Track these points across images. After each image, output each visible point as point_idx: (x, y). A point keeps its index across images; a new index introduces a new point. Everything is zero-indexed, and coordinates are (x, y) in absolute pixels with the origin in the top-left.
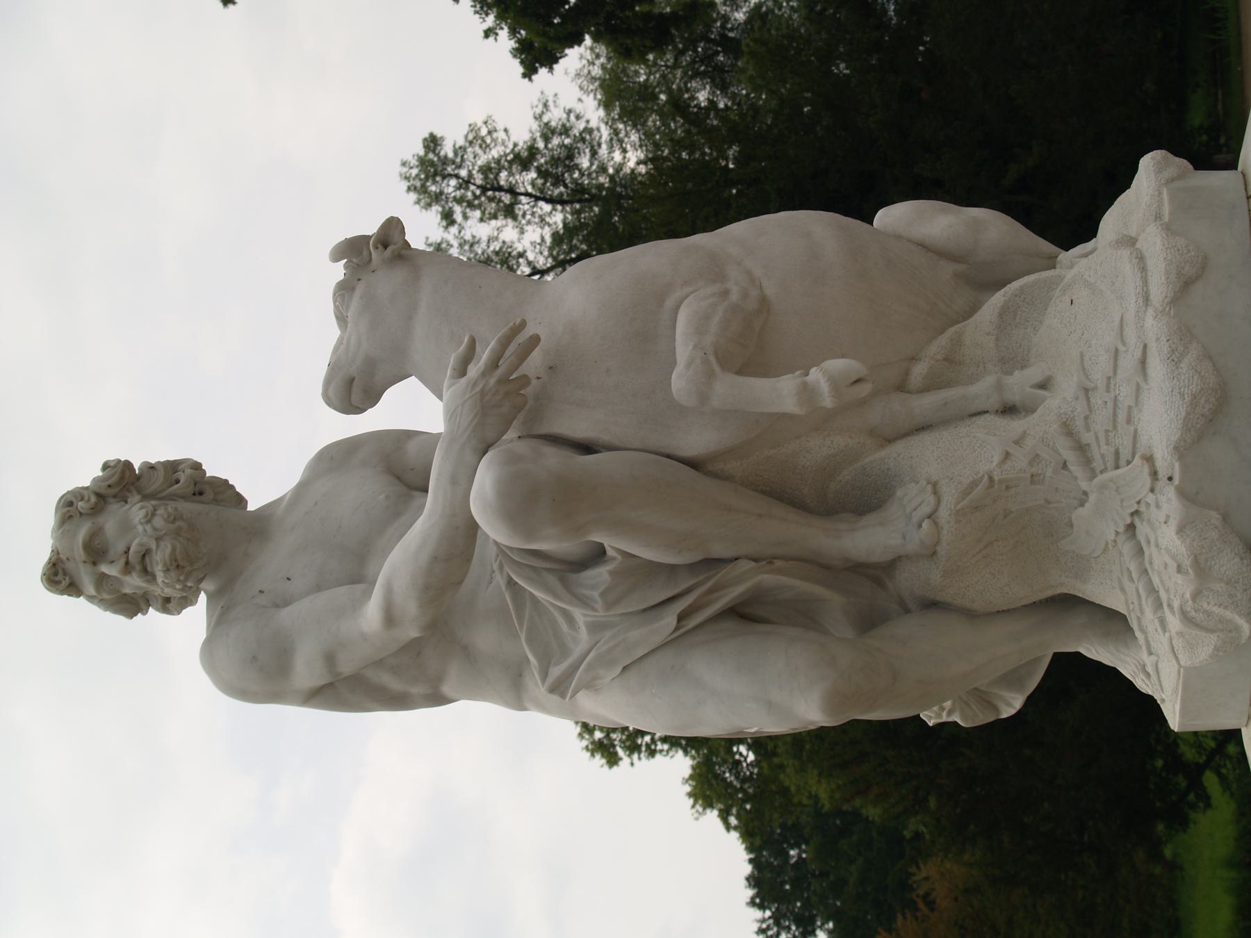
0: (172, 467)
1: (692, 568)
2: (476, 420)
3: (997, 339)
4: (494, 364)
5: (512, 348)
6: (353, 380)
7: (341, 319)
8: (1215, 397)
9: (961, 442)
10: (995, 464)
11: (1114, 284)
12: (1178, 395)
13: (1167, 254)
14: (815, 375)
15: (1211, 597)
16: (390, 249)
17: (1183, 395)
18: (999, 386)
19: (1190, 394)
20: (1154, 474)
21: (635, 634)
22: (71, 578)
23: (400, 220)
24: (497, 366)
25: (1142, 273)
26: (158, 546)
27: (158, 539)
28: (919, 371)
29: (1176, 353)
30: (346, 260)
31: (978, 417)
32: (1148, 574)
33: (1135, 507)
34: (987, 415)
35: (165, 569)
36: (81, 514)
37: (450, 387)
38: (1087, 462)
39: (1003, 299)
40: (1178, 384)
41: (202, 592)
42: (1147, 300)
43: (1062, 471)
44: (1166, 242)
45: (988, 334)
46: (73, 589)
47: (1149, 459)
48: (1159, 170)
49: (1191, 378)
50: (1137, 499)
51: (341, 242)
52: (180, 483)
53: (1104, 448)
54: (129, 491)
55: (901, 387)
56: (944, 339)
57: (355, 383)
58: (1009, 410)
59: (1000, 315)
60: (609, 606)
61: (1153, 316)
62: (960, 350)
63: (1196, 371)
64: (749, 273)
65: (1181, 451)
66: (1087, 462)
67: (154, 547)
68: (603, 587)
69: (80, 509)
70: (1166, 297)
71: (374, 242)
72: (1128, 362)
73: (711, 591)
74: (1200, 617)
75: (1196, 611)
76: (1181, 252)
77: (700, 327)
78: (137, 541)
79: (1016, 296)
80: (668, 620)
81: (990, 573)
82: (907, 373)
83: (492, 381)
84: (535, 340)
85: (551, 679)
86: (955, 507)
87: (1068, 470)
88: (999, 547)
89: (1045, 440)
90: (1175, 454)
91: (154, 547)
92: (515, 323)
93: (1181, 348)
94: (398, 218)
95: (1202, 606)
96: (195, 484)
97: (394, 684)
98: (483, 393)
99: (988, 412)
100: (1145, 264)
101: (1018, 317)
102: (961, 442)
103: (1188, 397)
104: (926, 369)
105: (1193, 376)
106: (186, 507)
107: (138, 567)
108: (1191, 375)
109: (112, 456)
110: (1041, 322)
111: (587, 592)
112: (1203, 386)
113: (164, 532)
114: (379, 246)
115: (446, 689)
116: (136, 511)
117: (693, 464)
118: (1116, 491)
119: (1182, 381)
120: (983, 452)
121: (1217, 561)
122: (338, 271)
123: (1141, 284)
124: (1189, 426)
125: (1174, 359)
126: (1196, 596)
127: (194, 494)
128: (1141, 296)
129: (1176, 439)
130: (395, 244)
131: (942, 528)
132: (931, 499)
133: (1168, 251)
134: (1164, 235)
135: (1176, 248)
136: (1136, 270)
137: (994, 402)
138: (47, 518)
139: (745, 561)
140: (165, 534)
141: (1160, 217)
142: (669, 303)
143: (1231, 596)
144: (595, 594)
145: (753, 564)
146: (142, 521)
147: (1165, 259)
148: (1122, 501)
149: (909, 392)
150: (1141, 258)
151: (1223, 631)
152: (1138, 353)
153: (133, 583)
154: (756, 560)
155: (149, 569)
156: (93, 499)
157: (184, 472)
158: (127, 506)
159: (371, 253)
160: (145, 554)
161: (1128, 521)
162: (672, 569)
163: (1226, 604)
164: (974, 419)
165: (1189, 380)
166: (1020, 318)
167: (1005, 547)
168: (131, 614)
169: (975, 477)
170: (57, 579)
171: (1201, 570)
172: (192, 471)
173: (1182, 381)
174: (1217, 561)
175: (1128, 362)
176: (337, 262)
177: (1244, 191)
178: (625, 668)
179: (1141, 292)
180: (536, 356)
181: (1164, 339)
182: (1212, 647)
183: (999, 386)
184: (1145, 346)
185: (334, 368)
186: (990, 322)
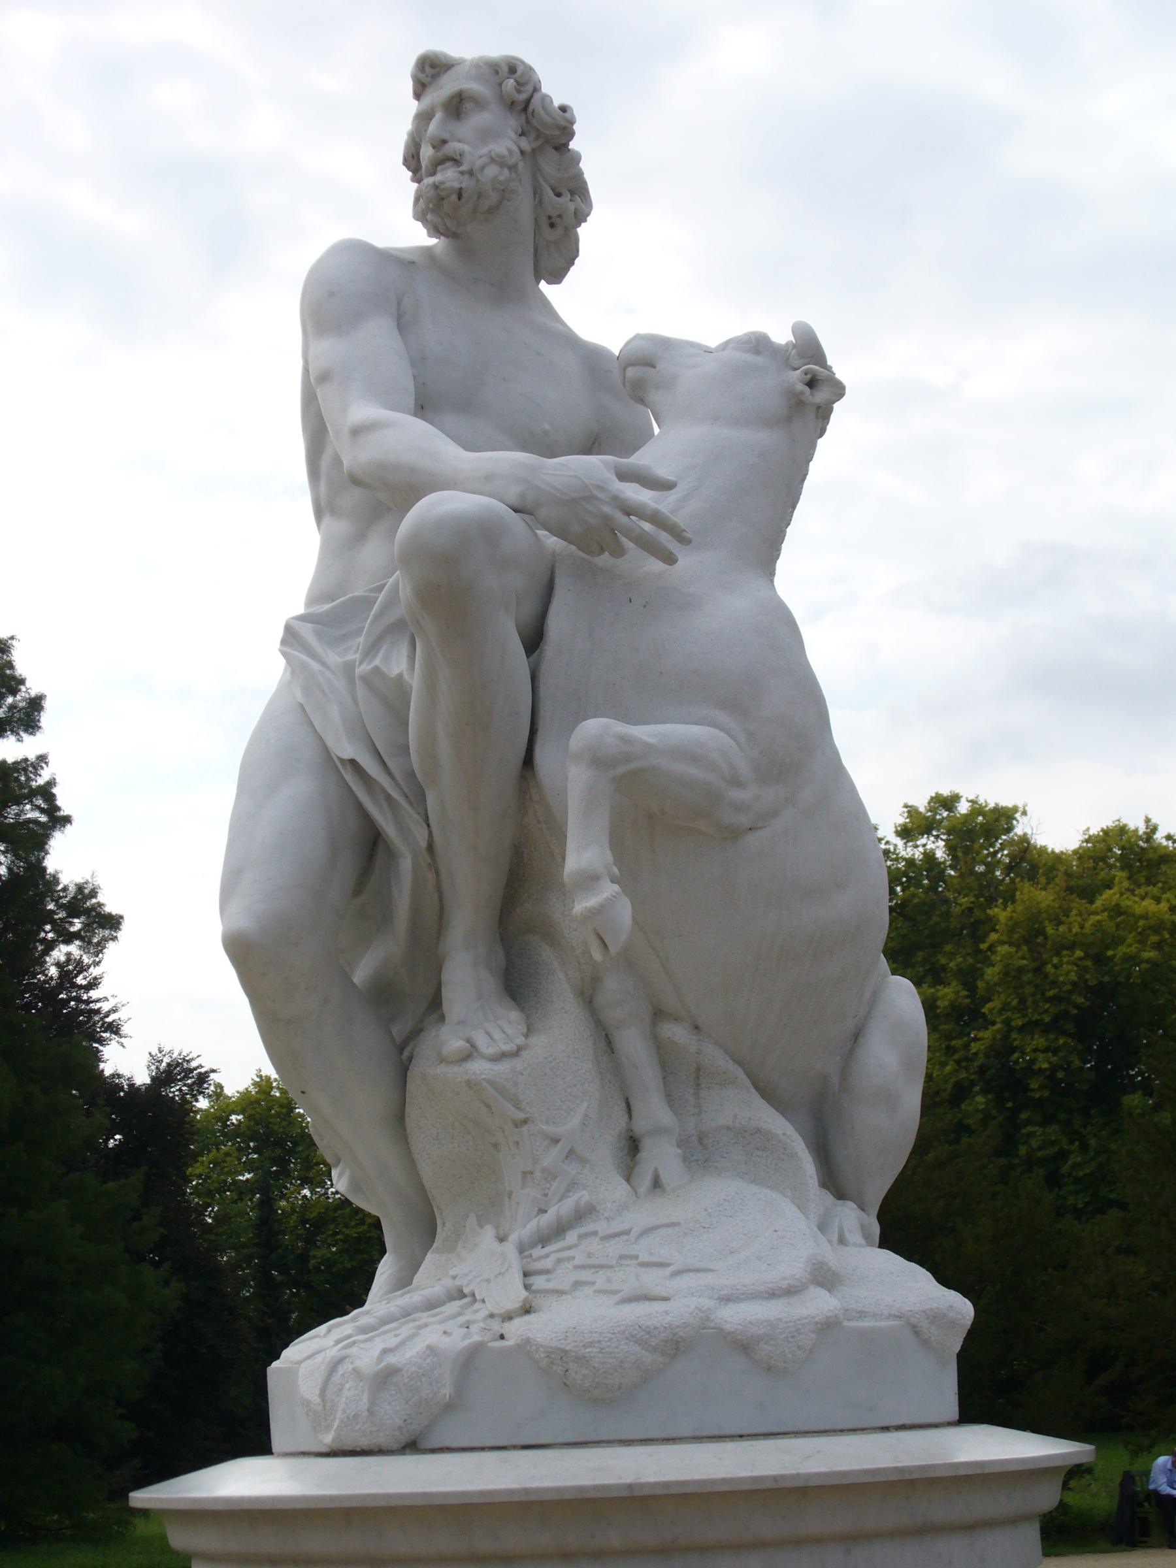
0: (577, 189)
1: (411, 774)
2: (558, 494)
3: (729, 1128)
4: (629, 510)
5: (647, 526)
6: (654, 367)
7: (725, 346)
8: (591, 1386)
9: (575, 1085)
10: (544, 1127)
11: (759, 1259)
12: (591, 1340)
13: (786, 1323)
14: (609, 889)
15: (356, 1392)
16: (807, 389)
17: (591, 1347)
18: (659, 1131)
19: (592, 1355)
20: (508, 1317)
21: (334, 712)
22: (431, 83)
23: (842, 397)
24: (629, 514)
25: (767, 1292)
26: (462, 173)
27: (471, 173)
28: (677, 1033)
29: (648, 1336)
30: (794, 342)
31: (625, 1108)
32: (404, 1317)
33: (478, 1297)
34: (626, 1117)
35: (437, 184)
36: (500, 84)
37: (603, 462)
38: (543, 1239)
39: (780, 1132)
40: (606, 1339)
41: (438, 240)
42: (727, 1299)
43: (537, 1209)
44: (806, 1321)
45: (735, 1116)
46: (420, 89)
47: (527, 1310)
48: (937, 1318)
49: (612, 1355)
50: (486, 1300)
51: (815, 334)
52: (557, 199)
53: (554, 1257)
54: (538, 137)
55: (659, 1014)
56: (722, 1061)
57: (649, 369)
58: (633, 1145)
59: (759, 1130)
60: (365, 679)
61: (703, 1307)
62: (716, 1084)
63: (622, 1362)
64: (774, 813)
65: (525, 1346)
66: (543, 1239)
67: (461, 169)
68: (384, 669)
69: (505, 82)
70: (726, 1321)
71: (811, 369)
72: (653, 1280)
73: (389, 798)
74: (336, 1378)
75: (343, 1375)
76: (790, 1339)
77: (691, 754)
78: (466, 148)
79: (785, 1149)
80: (346, 749)
81: (438, 1133)
82: (677, 1019)
83: (607, 509)
84: (670, 559)
85: (298, 625)
86: (484, 1079)
87: (538, 1214)
88: (467, 1142)
89: (576, 1186)
90: (522, 1340)
91: (461, 169)
92: (684, 530)
93: (653, 1342)
94: (844, 394)
95: (347, 1382)
96: (560, 216)
97: (325, 462)
98: (591, 498)
99: (630, 1117)
100: (780, 1296)
101: (760, 1153)
102: (575, 1085)
103: (589, 1352)
104: (681, 1041)
105: (615, 1357)
106: (523, 206)
107: (440, 154)
108: (617, 1355)
109: (579, 113)
110: (754, 1181)
111: (380, 655)
112: (602, 1371)
113: (481, 178)
114: (809, 376)
115: (327, 520)
116: (507, 144)
117: (528, 761)
118: (500, 1274)
119: (608, 1343)
120: (562, 1112)
121: (395, 1398)
122: (782, 336)
123: (749, 1292)
124: (553, 1356)
125: (641, 1336)
126: (356, 1371)
127: (550, 218)
128: (734, 1292)
129: (538, 1339)
130: (812, 394)
131: (460, 1066)
132: (491, 1051)
133: (791, 1324)
134: (817, 1319)
135: (795, 1334)
136: (769, 1286)
137: (641, 1125)
138: (496, 50)
139: (426, 833)
140: (478, 180)
141: (860, 1317)
142: (722, 716)
143: (356, 1416)
144: (377, 662)
145: (423, 844)
146: (493, 152)
147: (780, 1320)
148: (488, 1281)
149: (654, 1024)
150: (791, 1291)
151: (325, 1409)
152: (659, 1291)
153: (427, 152)
154: (431, 847)
155: (439, 168)
156: (522, 97)
157: (571, 200)
158: (513, 136)
159: (799, 369)
160: (455, 160)
161: (466, 1290)
162: (405, 749)
163: (348, 1412)
164: (624, 1104)
165: (610, 1353)
166: (758, 1156)
167: (468, 1150)
168: (406, 162)
169: (525, 1102)
170: (428, 69)
171: (385, 1378)
172: (573, 211)
173: (608, 1343)
174: (395, 1398)
175: (653, 1280)
176: (793, 332)
177: (900, 1422)
178: (302, 706)
179: (739, 1292)
180: (655, 565)
181: (668, 1319)
182: (310, 1398)
183: (659, 1131)
184: (666, 1299)
185: (666, 344)
186: (750, 1119)
